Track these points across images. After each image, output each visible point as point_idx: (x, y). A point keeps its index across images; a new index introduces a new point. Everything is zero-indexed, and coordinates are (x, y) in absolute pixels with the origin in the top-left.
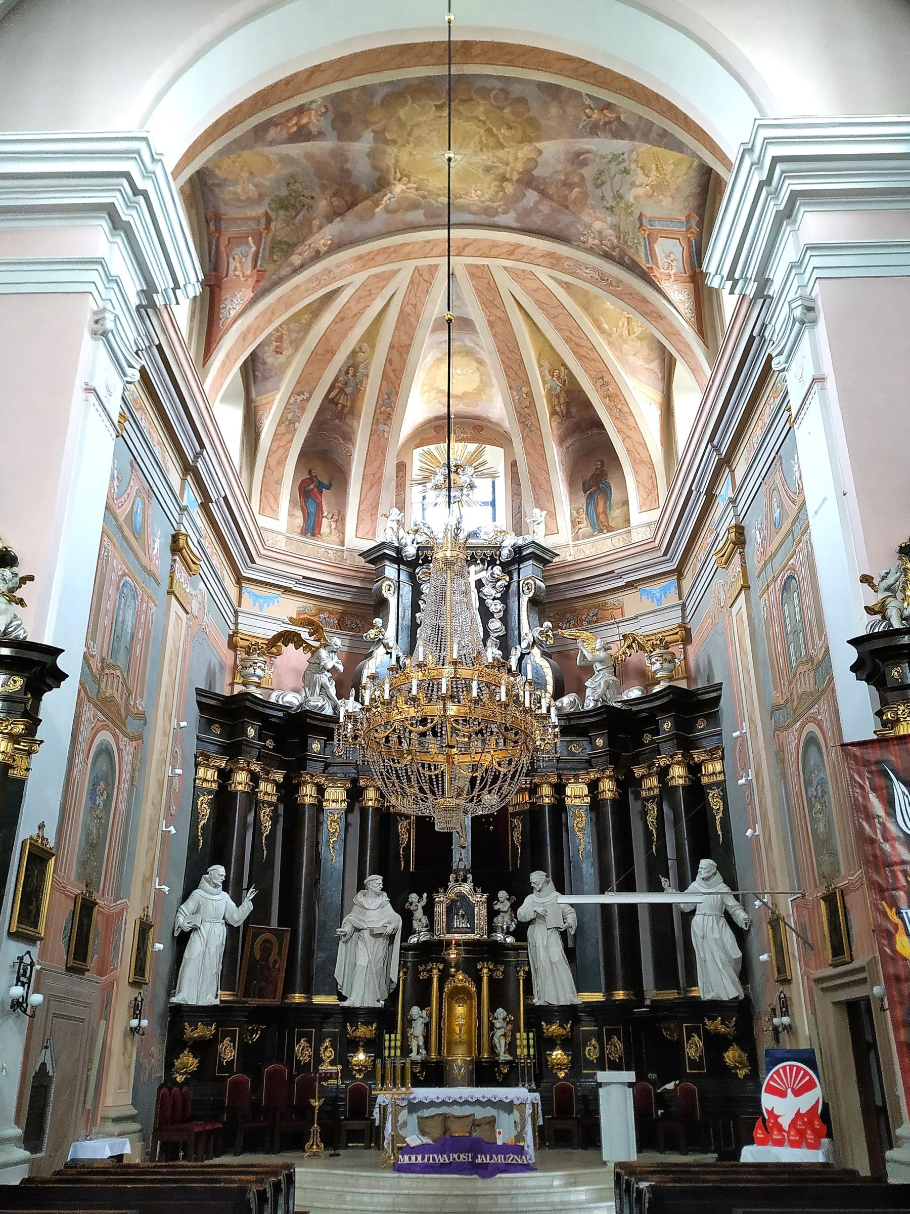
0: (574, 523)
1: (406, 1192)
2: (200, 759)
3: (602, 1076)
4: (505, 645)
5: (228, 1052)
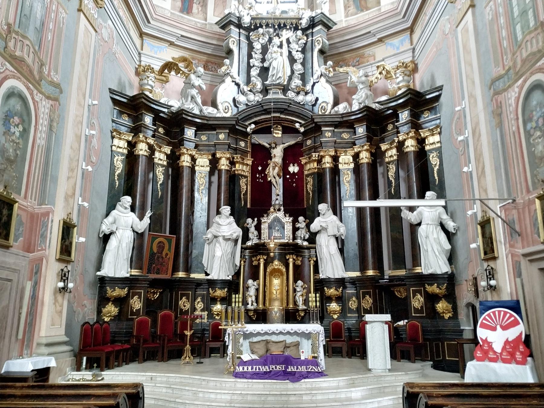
0: (346, 7)
1: (239, 392)
2: (114, 134)
3: (368, 317)
4: (303, 78)
5: (137, 304)
